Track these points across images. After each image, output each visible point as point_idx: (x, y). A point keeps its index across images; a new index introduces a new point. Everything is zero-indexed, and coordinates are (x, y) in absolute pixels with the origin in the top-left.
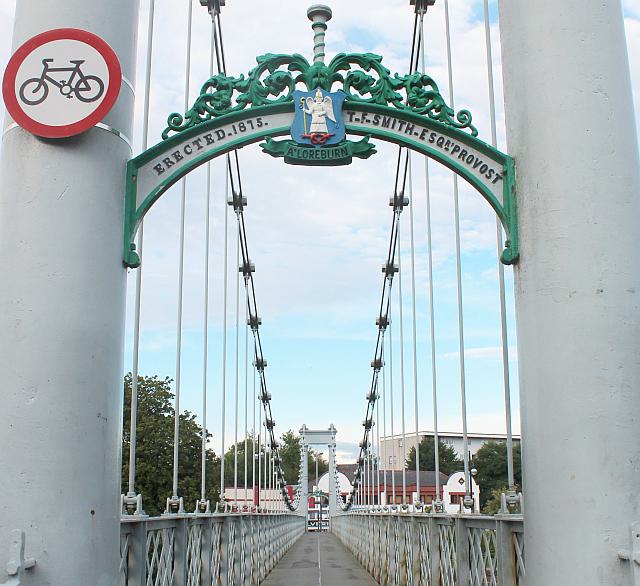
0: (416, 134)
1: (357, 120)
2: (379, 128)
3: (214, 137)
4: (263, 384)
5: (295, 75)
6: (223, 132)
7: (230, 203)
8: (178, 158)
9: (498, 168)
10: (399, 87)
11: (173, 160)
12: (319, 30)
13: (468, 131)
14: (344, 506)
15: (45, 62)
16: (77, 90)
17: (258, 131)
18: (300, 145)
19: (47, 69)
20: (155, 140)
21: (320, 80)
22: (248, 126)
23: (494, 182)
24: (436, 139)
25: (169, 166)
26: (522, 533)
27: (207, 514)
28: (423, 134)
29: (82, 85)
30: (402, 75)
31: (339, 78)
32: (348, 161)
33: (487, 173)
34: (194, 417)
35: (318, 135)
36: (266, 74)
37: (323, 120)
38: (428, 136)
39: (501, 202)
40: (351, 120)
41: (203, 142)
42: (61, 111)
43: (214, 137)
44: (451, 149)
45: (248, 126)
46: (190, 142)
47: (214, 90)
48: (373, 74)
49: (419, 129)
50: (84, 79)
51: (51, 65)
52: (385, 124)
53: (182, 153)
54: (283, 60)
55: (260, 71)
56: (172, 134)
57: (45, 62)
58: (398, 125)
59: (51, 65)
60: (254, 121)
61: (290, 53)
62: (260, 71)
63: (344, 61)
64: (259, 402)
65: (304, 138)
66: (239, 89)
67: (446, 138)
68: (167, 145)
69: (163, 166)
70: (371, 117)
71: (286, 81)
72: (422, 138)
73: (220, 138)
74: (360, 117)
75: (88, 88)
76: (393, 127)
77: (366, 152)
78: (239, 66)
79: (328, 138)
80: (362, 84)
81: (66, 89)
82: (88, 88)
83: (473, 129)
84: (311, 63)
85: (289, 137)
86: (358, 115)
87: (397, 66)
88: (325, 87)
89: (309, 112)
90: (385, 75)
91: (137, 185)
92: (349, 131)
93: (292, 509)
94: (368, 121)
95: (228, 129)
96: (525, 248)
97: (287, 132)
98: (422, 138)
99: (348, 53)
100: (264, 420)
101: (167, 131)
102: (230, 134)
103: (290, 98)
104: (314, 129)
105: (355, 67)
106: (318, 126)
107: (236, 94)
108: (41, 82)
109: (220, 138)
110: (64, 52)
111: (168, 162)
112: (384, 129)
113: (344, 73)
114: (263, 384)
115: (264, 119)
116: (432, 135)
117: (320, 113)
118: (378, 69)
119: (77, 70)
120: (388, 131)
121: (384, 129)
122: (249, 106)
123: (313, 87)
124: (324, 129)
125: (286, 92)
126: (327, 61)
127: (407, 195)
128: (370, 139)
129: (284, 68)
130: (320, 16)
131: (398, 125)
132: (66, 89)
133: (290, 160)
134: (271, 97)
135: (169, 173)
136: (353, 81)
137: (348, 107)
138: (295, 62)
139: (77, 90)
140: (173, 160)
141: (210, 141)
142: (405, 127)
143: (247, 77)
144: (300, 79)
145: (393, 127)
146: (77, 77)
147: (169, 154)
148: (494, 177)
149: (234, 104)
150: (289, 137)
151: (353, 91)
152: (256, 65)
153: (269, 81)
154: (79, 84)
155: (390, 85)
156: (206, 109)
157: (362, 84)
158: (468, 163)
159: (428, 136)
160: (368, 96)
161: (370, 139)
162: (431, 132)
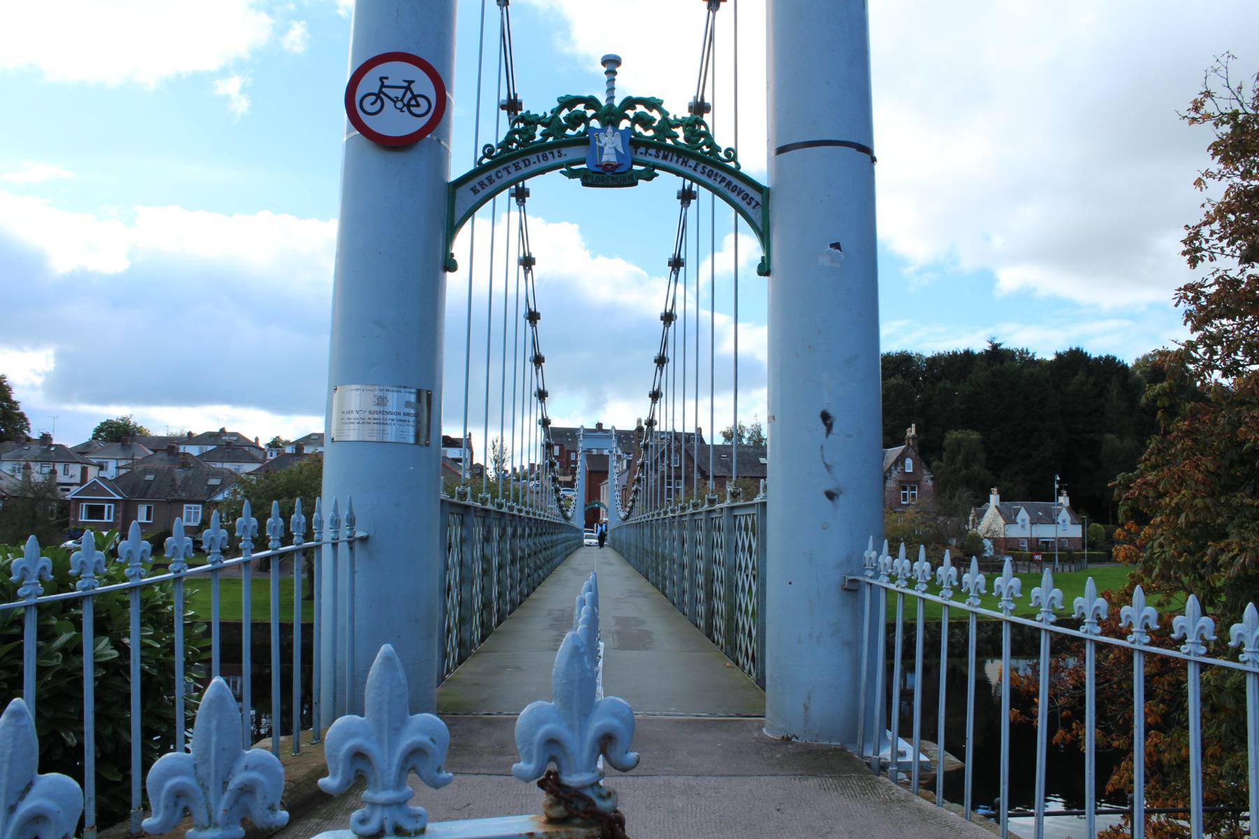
3: (522, 165)
4: (535, 344)
5: (590, 113)
7: (503, 107)
8: (490, 181)
9: (757, 196)
10: (677, 126)
11: (486, 182)
12: (611, 76)
13: (732, 164)
14: (622, 515)
15: (381, 79)
16: (408, 106)
17: (558, 160)
19: (383, 86)
20: (469, 166)
21: (611, 116)
22: (550, 156)
27: (489, 506)
29: (413, 102)
30: (679, 117)
31: (627, 117)
32: (635, 184)
34: (499, 461)
36: (565, 112)
37: (613, 151)
38: (700, 169)
39: (759, 224)
42: (394, 123)
43: (522, 165)
45: (550, 156)
46: (500, 168)
47: (522, 125)
48: (655, 114)
49: (692, 163)
50: (414, 97)
51: (386, 82)
52: (665, 157)
53: (494, 177)
54: (579, 100)
55: (560, 109)
56: (485, 161)
57: (381, 79)
59: (386, 82)
60: (555, 151)
61: (586, 95)
62: (560, 109)
63: (630, 102)
64: (530, 366)
66: (543, 125)
67: (715, 170)
68: (480, 170)
70: (653, 151)
71: (582, 118)
72: (695, 169)
75: (418, 105)
77: (650, 176)
78: (539, 103)
79: (617, 166)
80: (645, 122)
81: (399, 105)
82: (418, 105)
83: (737, 163)
84: (604, 104)
85: (585, 166)
86: (642, 150)
87: (678, 109)
88: (615, 125)
90: (664, 114)
91: (455, 204)
92: (634, 163)
93: (567, 518)
95: (533, 158)
97: (583, 162)
98: (695, 169)
99: (635, 95)
100: (535, 389)
101: (482, 159)
103: (585, 133)
104: (605, 159)
105: (640, 108)
106: (609, 157)
107: (540, 129)
108: (378, 96)
110: (398, 72)
113: (630, 113)
114: (535, 344)
115: (564, 151)
117: (610, 147)
118: (661, 111)
119: (408, 88)
122: (551, 139)
123: (605, 124)
125: (582, 128)
126: (617, 103)
127: (682, 256)
129: (580, 107)
130: (611, 63)
132: (399, 105)
133: (584, 184)
134: (569, 132)
135: (483, 193)
136: (640, 119)
137: (635, 143)
138: (591, 102)
139: (408, 106)
140: (486, 182)
141: (517, 168)
143: (549, 115)
144: (593, 117)
146: (409, 95)
147: (483, 177)
149: (538, 138)
150: (585, 166)
151: (638, 128)
152: (557, 104)
153: (567, 118)
154: (409, 103)
155: (667, 125)
156: (515, 141)
157: (645, 122)
159: (700, 169)
160: (650, 133)
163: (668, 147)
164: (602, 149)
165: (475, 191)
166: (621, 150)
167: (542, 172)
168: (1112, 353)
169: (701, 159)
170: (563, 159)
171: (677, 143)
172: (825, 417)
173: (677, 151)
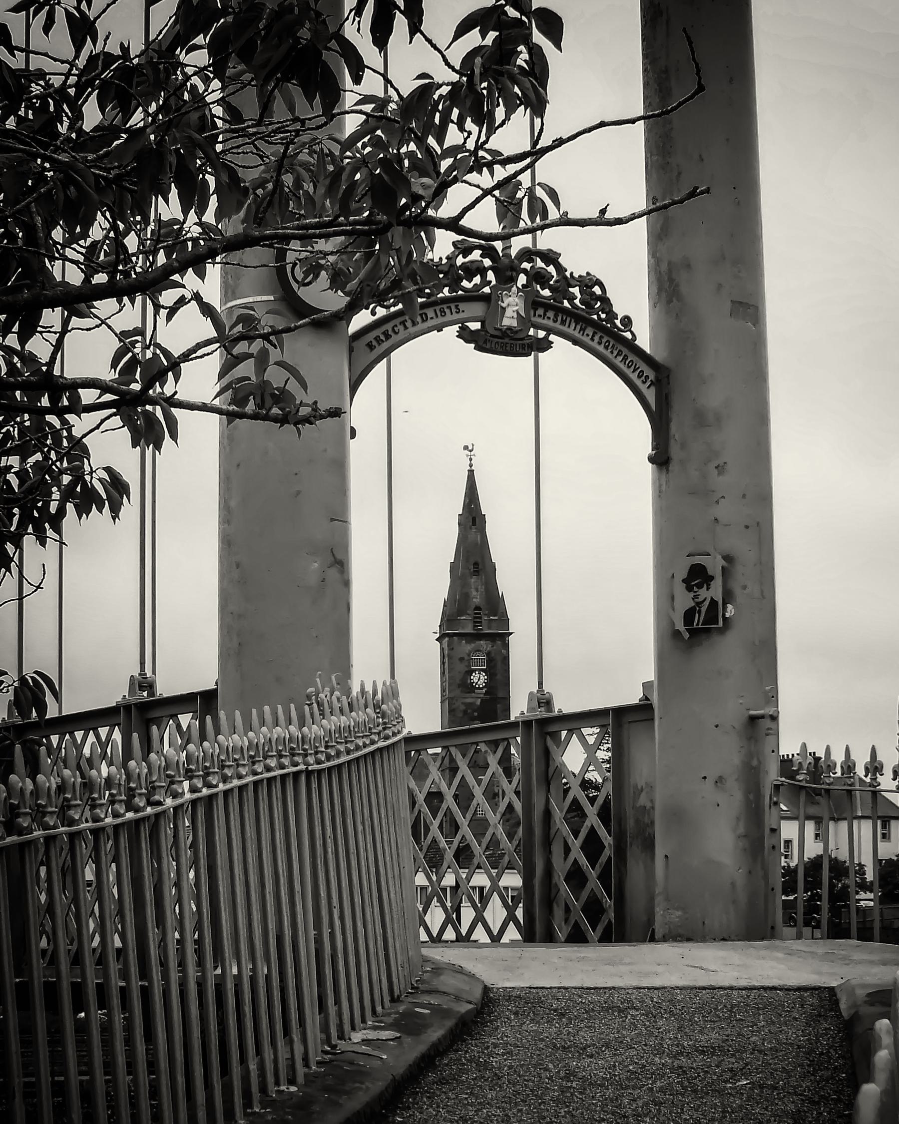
0: (588, 335)
1: (540, 316)
2: (558, 326)
6: (426, 314)
8: (388, 337)
13: (628, 335)
18: (492, 336)
23: (649, 387)
24: (604, 340)
25: (379, 344)
26: (774, 718)
28: (593, 336)
33: (643, 378)
35: (510, 328)
37: (515, 315)
40: (535, 315)
41: (409, 324)
44: (615, 353)
52: (563, 323)
58: (573, 325)
60: (453, 306)
65: (496, 329)
69: (374, 343)
73: (423, 321)
74: (542, 314)
76: (569, 326)
79: (517, 332)
89: (504, 305)
90: (560, 269)
94: (549, 318)
96: (675, 451)
102: (432, 318)
104: (506, 322)
106: (509, 321)
109: (423, 321)
111: (377, 339)
112: (561, 327)
115: (462, 306)
116: (601, 337)
120: (565, 329)
121: (561, 327)
124: (514, 323)
125: (477, 280)
126: (513, 252)
128: (479, 327)
131: (573, 325)
133: (479, 348)
134: (465, 283)
140: (382, 337)
142: (578, 327)
144: (491, 268)
145: (569, 326)
147: (377, 332)
148: (648, 383)
155: (566, 281)
157: (538, 277)
158: (629, 367)
159: (597, 338)
161: (479, 327)
162: (600, 334)
163: (565, 311)
164: (504, 309)
165: (370, 346)
166: (523, 314)
167: (575, 342)
168: (543, 6)
169: (597, 326)
170: (461, 315)
171: (574, 306)
172: (666, 856)
173: (574, 316)
